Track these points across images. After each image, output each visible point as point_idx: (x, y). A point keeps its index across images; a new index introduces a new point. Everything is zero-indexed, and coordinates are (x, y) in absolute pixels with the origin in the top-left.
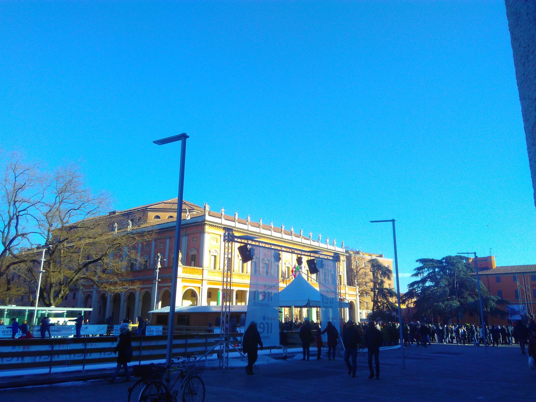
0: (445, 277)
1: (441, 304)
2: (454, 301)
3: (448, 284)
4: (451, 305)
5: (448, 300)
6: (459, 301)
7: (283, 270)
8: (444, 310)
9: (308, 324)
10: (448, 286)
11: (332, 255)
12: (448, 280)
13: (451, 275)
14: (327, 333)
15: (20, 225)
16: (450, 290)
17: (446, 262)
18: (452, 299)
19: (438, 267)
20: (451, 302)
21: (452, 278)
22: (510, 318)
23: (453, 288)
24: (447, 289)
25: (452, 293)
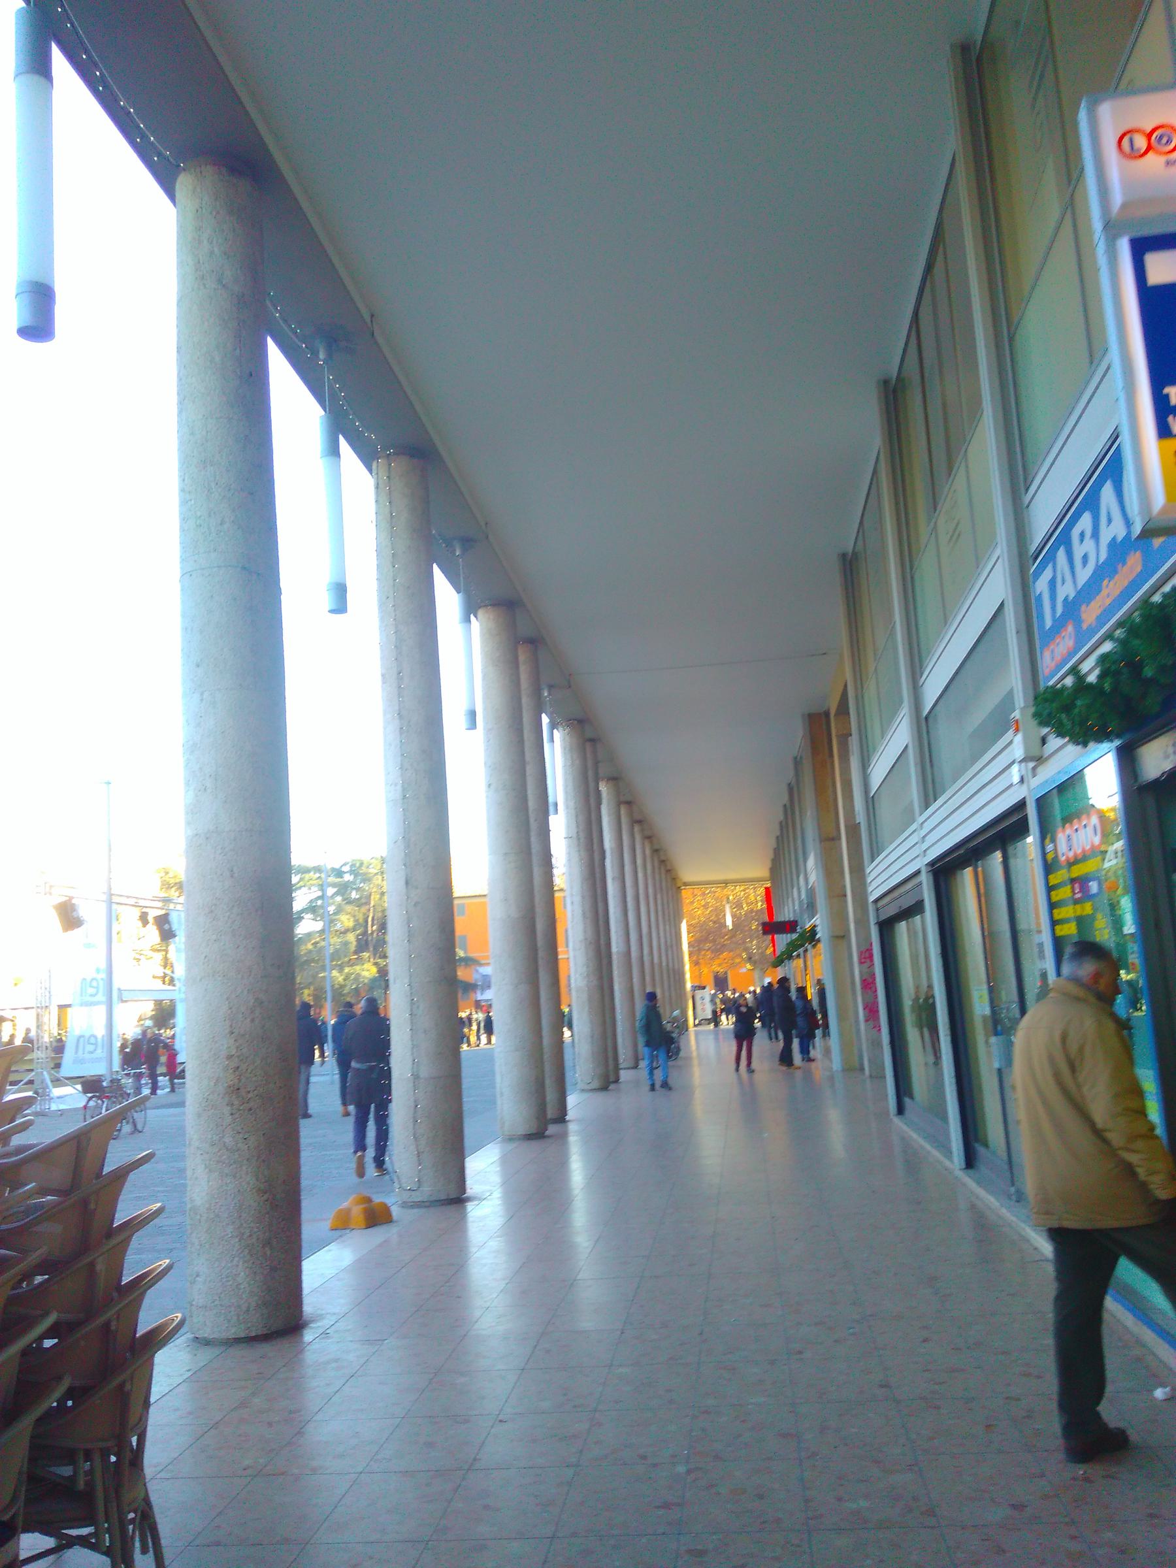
0: (349, 908)
1: (335, 973)
2: (366, 966)
3: (355, 926)
4: (359, 975)
5: (351, 964)
6: (376, 964)
7: (132, 1176)
8: (342, 986)
9: (27, 1491)
10: (354, 929)
11: (676, 967)
12: (354, 916)
13: (358, 903)
14: (57, 1343)
15: (907, 922)
16: (358, 940)
17: (351, 872)
18: (360, 961)
19: (334, 885)
20: (358, 968)
21: (364, 909)
22: (479, 997)
23: (365, 933)
24: (351, 938)
25: (362, 946)
